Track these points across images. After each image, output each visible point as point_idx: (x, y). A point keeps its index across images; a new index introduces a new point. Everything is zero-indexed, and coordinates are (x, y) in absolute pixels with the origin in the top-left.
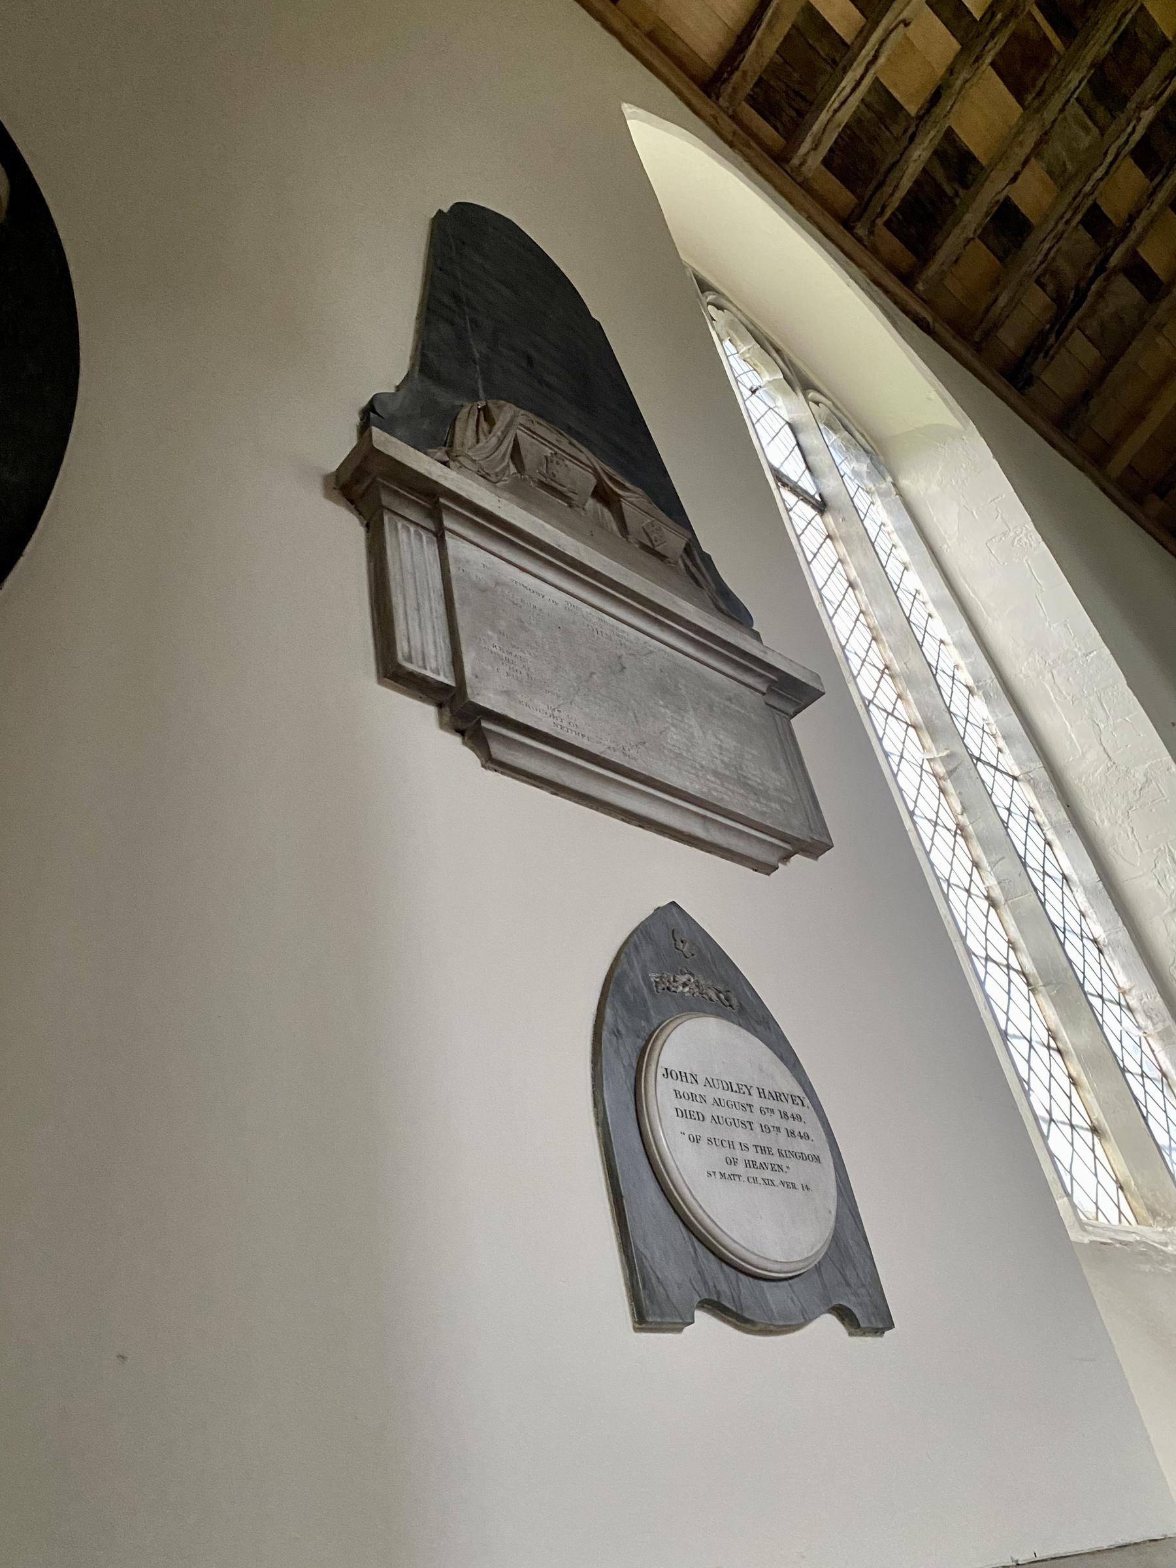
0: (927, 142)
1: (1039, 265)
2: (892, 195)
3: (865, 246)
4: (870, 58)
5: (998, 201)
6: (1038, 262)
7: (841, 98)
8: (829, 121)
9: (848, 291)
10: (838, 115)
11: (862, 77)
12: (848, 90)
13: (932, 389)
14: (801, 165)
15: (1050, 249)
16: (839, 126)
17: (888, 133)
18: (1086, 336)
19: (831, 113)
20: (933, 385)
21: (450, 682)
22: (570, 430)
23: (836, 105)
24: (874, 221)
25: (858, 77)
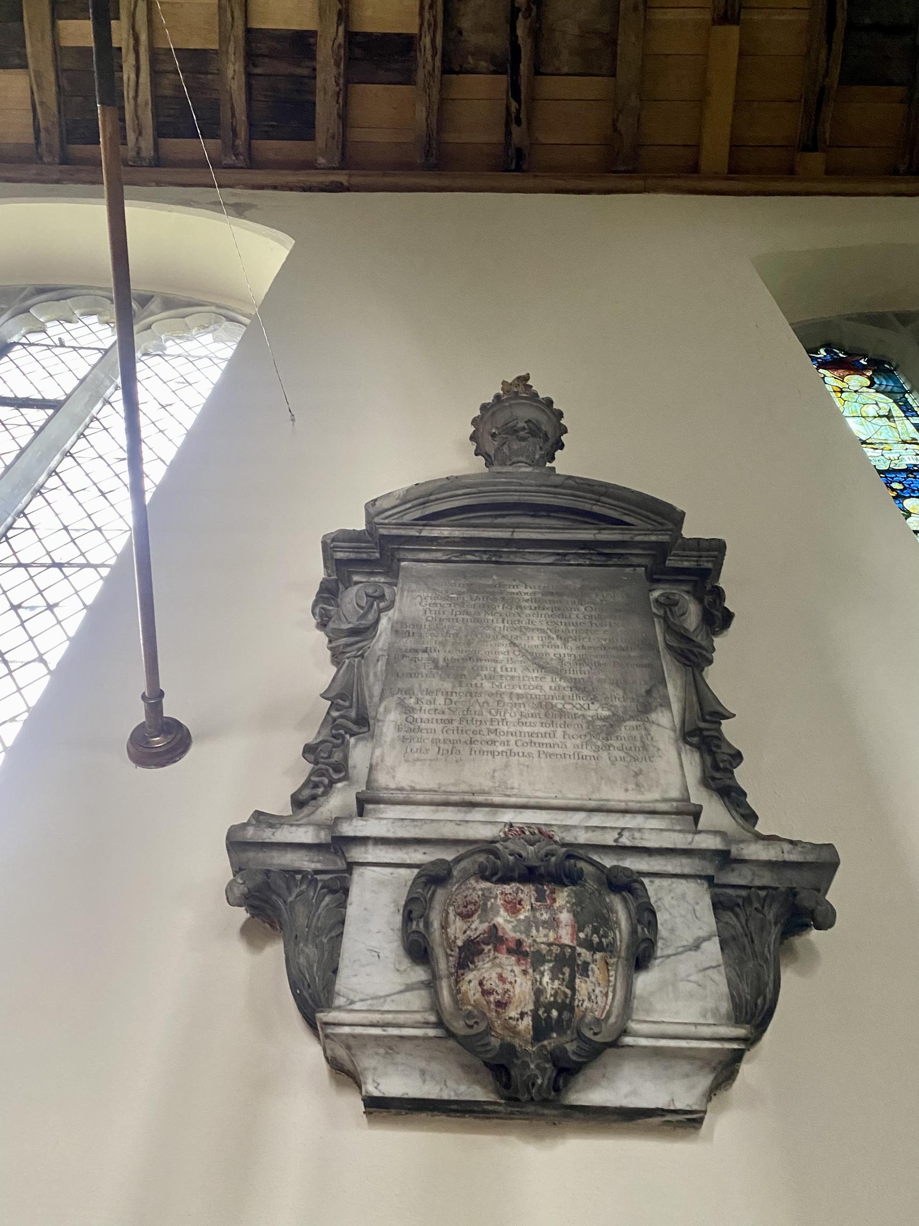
0: (232, 58)
1: (433, 59)
2: (233, 115)
3: (242, 168)
4: (132, 42)
5: (339, 46)
6: (430, 59)
7: (132, 83)
8: (136, 105)
9: (174, 215)
10: (140, 99)
11: (137, 59)
12: (133, 76)
13: (268, 239)
14: (138, 153)
15: (433, 41)
16: (146, 104)
17: (210, 77)
18: (567, 74)
19: (132, 102)
20: (266, 236)
21: (416, 871)
22: (532, 516)
23: (132, 94)
24: (233, 145)
25: (134, 62)
